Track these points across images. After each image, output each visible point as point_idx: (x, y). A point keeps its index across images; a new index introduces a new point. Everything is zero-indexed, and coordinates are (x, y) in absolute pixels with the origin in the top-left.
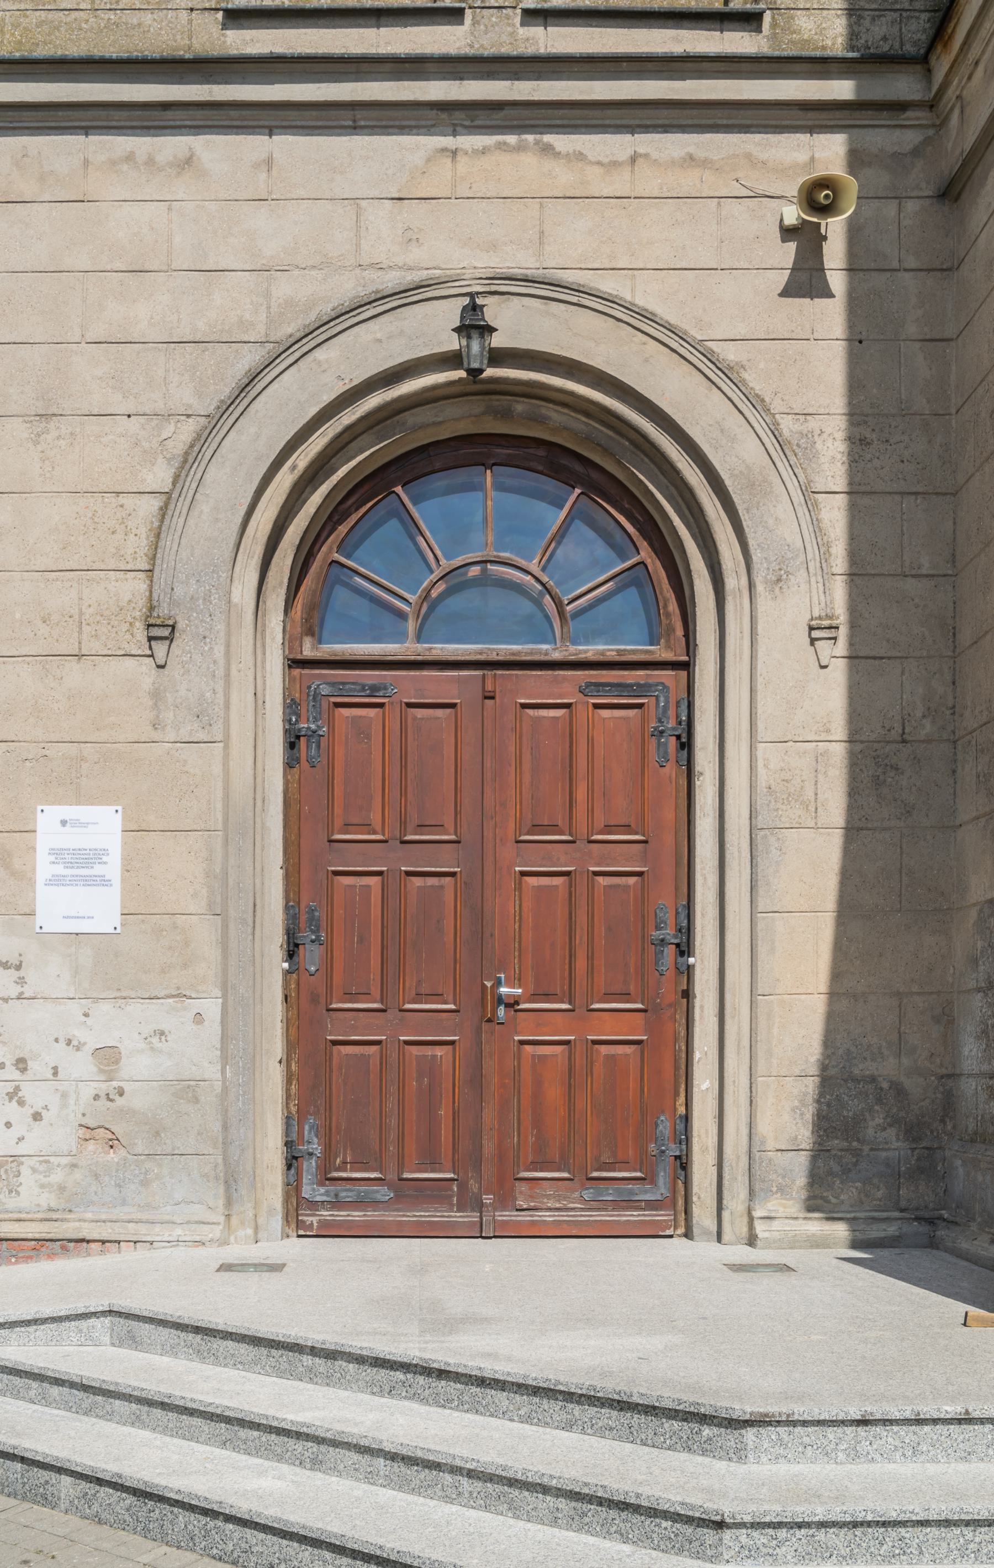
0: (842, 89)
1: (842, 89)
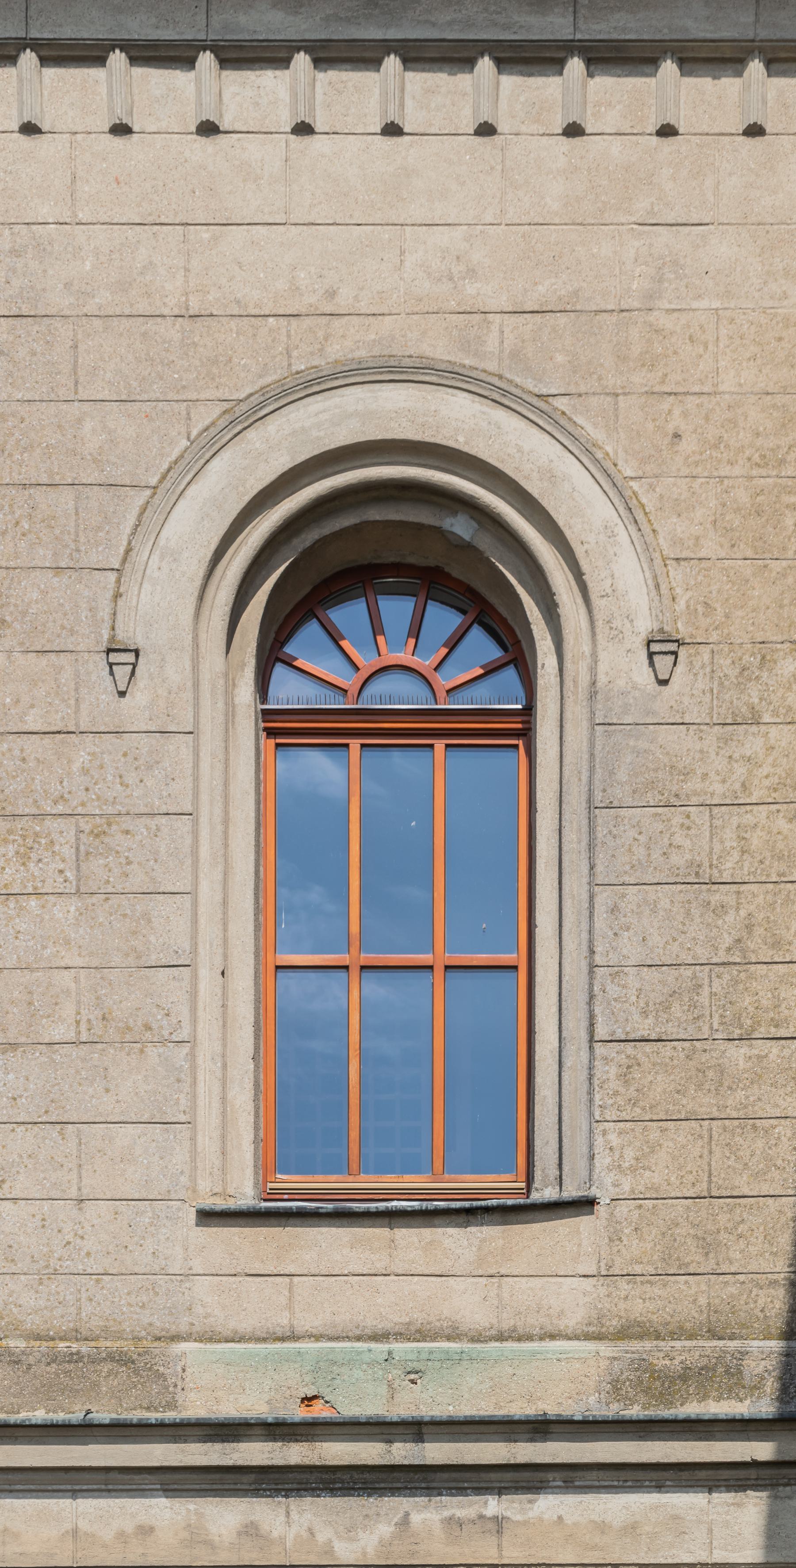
0: (762, 1450)
1: (762, 1450)
